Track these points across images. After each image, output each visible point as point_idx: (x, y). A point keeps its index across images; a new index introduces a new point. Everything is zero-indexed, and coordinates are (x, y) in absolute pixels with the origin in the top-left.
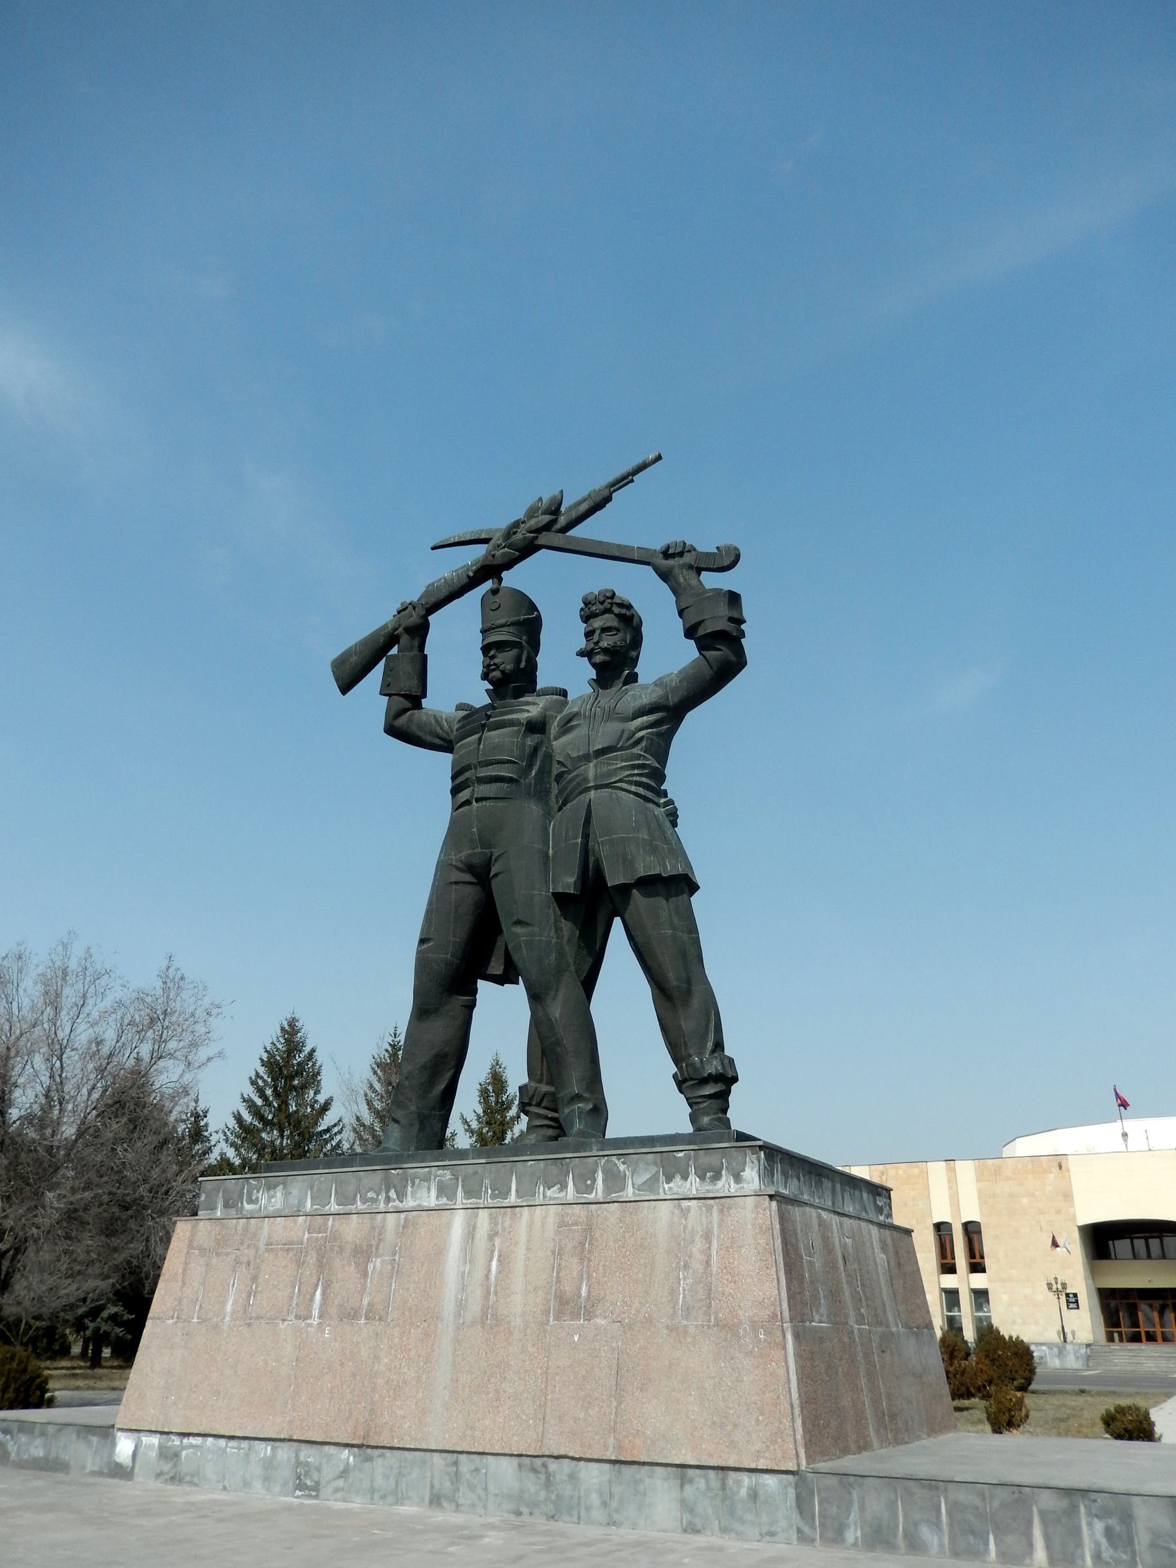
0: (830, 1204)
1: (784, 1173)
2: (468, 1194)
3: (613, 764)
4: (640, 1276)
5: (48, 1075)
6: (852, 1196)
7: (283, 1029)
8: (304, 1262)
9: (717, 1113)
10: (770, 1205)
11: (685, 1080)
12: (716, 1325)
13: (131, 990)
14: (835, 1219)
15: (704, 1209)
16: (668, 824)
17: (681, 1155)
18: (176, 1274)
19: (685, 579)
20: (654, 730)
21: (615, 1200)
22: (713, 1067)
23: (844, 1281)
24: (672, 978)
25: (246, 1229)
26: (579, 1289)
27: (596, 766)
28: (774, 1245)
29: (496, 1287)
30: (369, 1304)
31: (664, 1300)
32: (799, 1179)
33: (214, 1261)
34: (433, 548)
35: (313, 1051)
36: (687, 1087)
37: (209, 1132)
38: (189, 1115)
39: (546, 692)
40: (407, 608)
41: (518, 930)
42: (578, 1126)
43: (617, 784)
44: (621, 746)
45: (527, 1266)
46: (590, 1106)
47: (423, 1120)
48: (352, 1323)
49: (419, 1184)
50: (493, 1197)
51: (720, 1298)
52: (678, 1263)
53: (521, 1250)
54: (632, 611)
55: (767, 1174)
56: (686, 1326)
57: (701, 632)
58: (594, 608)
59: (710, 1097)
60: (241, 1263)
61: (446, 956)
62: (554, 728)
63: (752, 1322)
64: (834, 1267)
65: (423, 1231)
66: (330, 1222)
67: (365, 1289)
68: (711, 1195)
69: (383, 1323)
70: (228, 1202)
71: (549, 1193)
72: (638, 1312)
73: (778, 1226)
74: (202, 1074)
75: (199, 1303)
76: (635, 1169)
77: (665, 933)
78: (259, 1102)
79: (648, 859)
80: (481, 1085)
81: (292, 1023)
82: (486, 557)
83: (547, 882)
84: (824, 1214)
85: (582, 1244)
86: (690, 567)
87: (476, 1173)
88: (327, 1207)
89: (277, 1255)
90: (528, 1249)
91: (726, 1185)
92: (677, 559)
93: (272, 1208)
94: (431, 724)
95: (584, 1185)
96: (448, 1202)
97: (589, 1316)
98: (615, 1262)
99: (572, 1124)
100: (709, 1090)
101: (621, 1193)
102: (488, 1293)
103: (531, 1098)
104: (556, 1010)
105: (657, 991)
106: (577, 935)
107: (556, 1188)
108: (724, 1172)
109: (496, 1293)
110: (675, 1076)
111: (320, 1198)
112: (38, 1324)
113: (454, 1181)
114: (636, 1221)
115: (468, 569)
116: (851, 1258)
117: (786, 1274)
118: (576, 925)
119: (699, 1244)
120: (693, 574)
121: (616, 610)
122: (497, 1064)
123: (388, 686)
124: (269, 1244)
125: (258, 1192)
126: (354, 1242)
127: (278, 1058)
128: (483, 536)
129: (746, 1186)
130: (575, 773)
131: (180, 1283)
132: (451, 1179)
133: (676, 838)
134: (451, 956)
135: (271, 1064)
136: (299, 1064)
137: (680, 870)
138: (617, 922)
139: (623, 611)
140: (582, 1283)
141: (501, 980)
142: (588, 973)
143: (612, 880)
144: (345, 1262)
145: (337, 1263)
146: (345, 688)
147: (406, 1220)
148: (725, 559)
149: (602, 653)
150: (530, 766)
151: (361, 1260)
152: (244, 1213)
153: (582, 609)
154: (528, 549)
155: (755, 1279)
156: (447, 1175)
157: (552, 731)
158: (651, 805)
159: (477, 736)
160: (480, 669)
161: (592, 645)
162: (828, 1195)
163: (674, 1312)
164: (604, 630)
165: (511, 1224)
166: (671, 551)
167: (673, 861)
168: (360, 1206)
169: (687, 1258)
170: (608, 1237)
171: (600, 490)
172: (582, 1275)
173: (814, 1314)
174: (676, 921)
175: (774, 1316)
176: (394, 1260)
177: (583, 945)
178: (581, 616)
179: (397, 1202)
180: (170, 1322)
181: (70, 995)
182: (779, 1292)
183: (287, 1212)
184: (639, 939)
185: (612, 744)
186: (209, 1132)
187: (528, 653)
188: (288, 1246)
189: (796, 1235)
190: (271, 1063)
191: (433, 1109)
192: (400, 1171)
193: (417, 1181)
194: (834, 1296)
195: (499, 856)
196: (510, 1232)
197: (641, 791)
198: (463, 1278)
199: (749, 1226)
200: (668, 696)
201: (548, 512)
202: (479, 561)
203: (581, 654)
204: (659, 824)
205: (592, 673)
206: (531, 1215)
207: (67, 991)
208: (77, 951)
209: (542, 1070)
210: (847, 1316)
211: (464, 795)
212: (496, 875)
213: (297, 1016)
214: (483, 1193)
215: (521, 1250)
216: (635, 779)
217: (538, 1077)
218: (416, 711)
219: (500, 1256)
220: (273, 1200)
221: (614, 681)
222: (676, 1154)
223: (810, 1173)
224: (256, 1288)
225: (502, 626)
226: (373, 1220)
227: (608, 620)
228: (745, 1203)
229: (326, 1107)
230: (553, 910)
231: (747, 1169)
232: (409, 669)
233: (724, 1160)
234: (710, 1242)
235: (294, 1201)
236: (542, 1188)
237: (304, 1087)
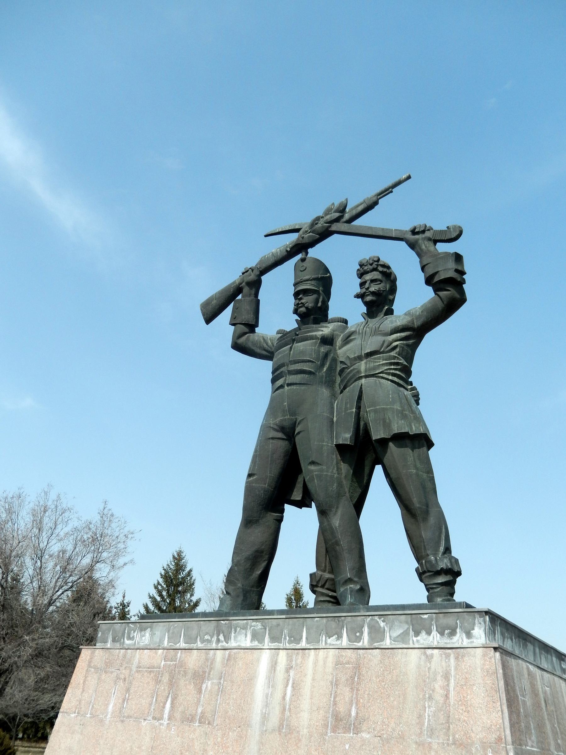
0: (532, 659)
1: (502, 634)
2: (274, 639)
3: (377, 362)
4: (395, 703)
5: (33, 568)
6: (546, 658)
7: (174, 557)
8: (160, 681)
9: (447, 596)
10: (494, 654)
11: (424, 572)
12: (454, 743)
13: (83, 522)
14: (538, 672)
15: (444, 656)
16: (413, 401)
18: (79, 684)
19: (426, 247)
20: (405, 342)
21: (377, 647)
22: (444, 564)
23: (546, 718)
24: (416, 502)
25: (125, 656)
26: (350, 711)
27: (366, 363)
28: (498, 685)
29: (290, 705)
30: (202, 713)
31: (414, 722)
32: (512, 640)
33: (103, 676)
34: (266, 236)
35: (191, 571)
36: (426, 577)
37: (130, 615)
38: (119, 605)
39: (334, 320)
40: (248, 271)
41: (312, 467)
42: (349, 599)
43: (380, 375)
45: (312, 692)
46: (358, 587)
47: (246, 593)
48: (190, 725)
49: (239, 631)
50: (290, 642)
51: (457, 723)
52: (425, 695)
53: (309, 679)
54: (390, 270)
55: (491, 632)
56: (430, 743)
57: (436, 279)
58: (366, 268)
59: (442, 584)
60: (120, 679)
62: (339, 342)
63: (483, 743)
64: (539, 706)
65: (240, 663)
66: (179, 655)
67: (200, 702)
68: (449, 646)
69: (210, 726)
70: (115, 638)
71: (329, 641)
72: (394, 730)
73: (501, 671)
74: (121, 573)
75: (92, 704)
76: (392, 626)
78: (159, 599)
79: (400, 422)
80: (287, 595)
81: (179, 553)
82: (298, 239)
83: (332, 438)
84: (531, 668)
85: (352, 678)
86: (429, 239)
87: (278, 625)
88: (178, 645)
89: (143, 674)
90: (313, 679)
91: (459, 639)
92: (420, 235)
93: (142, 644)
94: (260, 342)
95: (356, 634)
96: (258, 645)
97: (357, 731)
98: (376, 692)
99: (346, 597)
100: (441, 579)
101: (382, 643)
102: (284, 709)
103: (318, 582)
104: (336, 521)
105: (405, 511)
107: (334, 637)
108: (458, 630)
109: (290, 709)
110: (417, 570)
111: (174, 638)
112: (26, 719)
113: (263, 630)
114: (392, 663)
115: (287, 247)
116: (550, 702)
117: (508, 707)
118: (351, 466)
119: (439, 684)
120: (431, 244)
121: (380, 269)
122: (298, 583)
123: (235, 318)
124: (139, 667)
125: (134, 632)
126: (194, 669)
127: (171, 574)
128: (297, 227)
129: (475, 640)
130: (352, 368)
131: (81, 690)
132: (261, 629)
133: (419, 411)
134: (268, 486)
135: (166, 577)
136: (182, 578)
137: (422, 431)
138: (378, 469)
139: (385, 270)
140: (351, 707)
141: (300, 504)
142: (358, 499)
143: (377, 434)
144: (187, 682)
145: (182, 682)
146: (208, 321)
147: (229, 655)
148: (453, 233)
149: (371, 295)
150: (323, 365)
151: (198, 682)
152: (125, 646)
153: (358, 270)
154: (325, 234)
155: (484, 711)
156: (258, 626)
157: (338, 344)
158: (402, 389)
159: (289, 346)
160: (292, 307)
161: (364, 290)
162: (531, 654)
163: (421, 732)
164: (372, 281)
165: (302, 662)
166: (416, 230)
167: (417, 425)
168: (199, 645)
169: (431, 692)
170: (372, 674)
171: (371, 198)
172: (352, 701)
173: (528, 740)
174: (418, 465)
175: (499, 739)
176: (220, 683)
177: (355, 480)
178: (358, 275)
179: (224, 643)
180: (73, 715)
181: (47, 522)
182: (503, 721)
183: (152, 646)
184: (393, 476)
185: (377, 349)
186: (130, 615)
187: (323, 298)
188: (151, 669)
189: (513, 679)
190: (166, 577)
191: (252, 587)
192: (227, 622)
193: (238, 629)
194: (540, 727)
195: (300, 421)
196: (301, 667)
197: (395, 379)
198: (267, 699)
199: (479, 670)
200: (413, 321)
201: (337, 211)
202: (293, 242)
203: (358, 296)
204: (407, 400)
205: (364, 309)
206: (316, 656)
207: (46, 520)
208: (53, 496)
209: (325, 563)
210: (549, 744)
211: (280, 382)
212: (299, 433)
213: (182, 550)
214: (283, 639)
215: (309, 679)
216: (391, 371)
217: (323, 568)
218: (251, 334)
219: (293, 683)
220: (143, 638)
221: (378, 313)
222: (422, 616)
223: (519, 637)
224: (129, 696)
225: (307, 280)
226: (207, 654)
227: (375, 275)
228: (475, 653)
229: (196, 604)
230: (336, 456)
231: (476, 628)
232: (248, 307)
233: (458, 622)
234: (448, 680)
235: (156, 639)
236: (324, 637)
237: (185, 592)
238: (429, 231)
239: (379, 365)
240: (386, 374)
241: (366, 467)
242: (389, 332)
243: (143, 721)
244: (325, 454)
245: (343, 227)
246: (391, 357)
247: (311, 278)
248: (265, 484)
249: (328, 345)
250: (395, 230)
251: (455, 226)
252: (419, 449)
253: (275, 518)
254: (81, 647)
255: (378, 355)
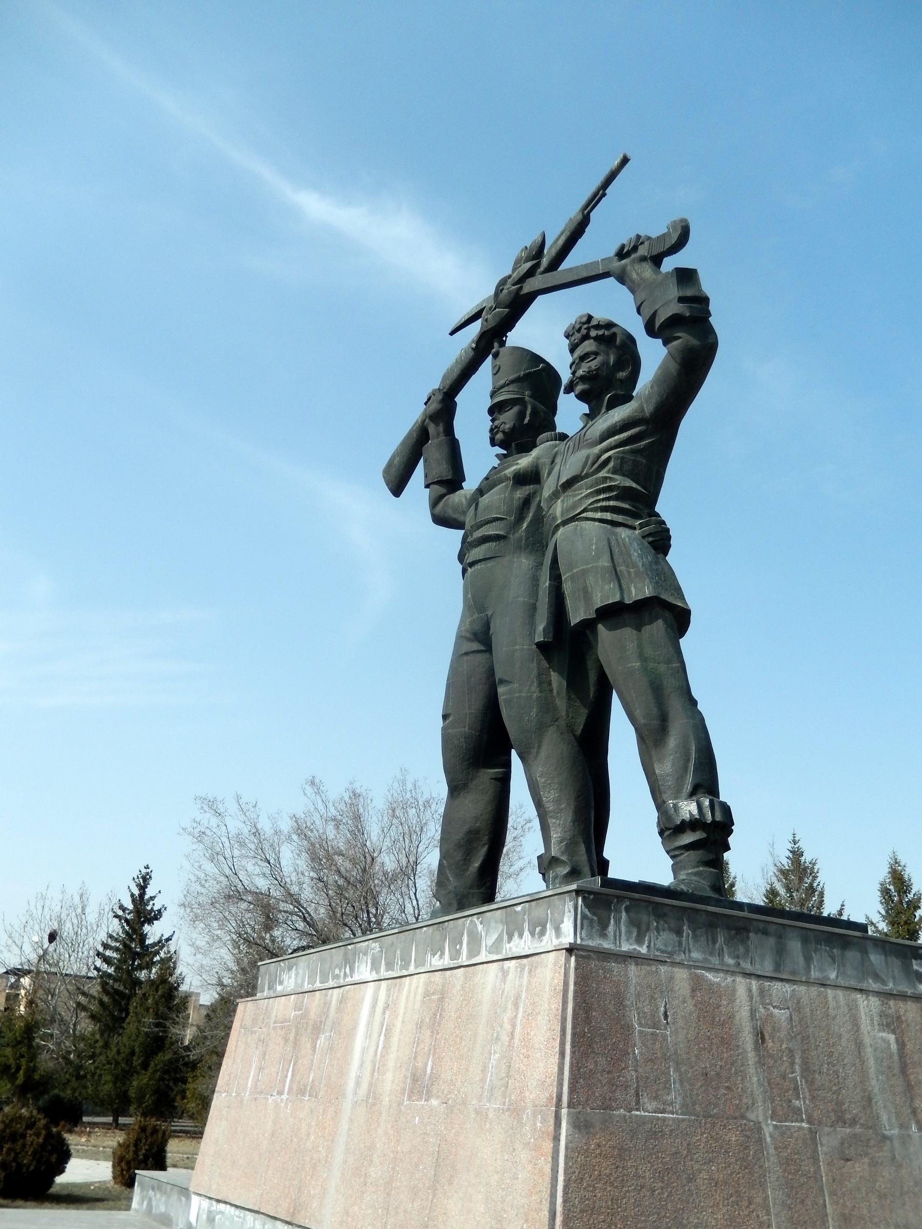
3: (579, 494)
9: (698, 867)
17: (519, 908)
19: (637, 274)
27: (563, 501)
34: (452, 333)
44: (586, 474)
57: (658, 323)
61: (463, 729)
76: (488, 930)
77: (632, 667)
79: (607, 587)
86: (643, 259)
90: (403, 1022)
102: (374, 1070)
106: (565, 687)
113: (380, 953)
122: (896, 863)
131: (232, 1060)
134: (469, 729)
140: (429, 1060)
142: (584, 725)
149: (580, 383)
197: (608, 516)
216: (600, 504)
238: (643, 245)
239: (581, 499)
240: (592, 511)
241: (589, 672)
242: (598, 438)
243: (269, 1097)
244: (518, 665)
245: (537, 283)
246: (598, 481)
247: (507, 382)
248: (465, 728)
249: (530, 485)
250: (603, 260)
251: (675, 221)
252: (650, 624)
253: (494, 777)
254: (238, 1001)
255: (579, 482)
